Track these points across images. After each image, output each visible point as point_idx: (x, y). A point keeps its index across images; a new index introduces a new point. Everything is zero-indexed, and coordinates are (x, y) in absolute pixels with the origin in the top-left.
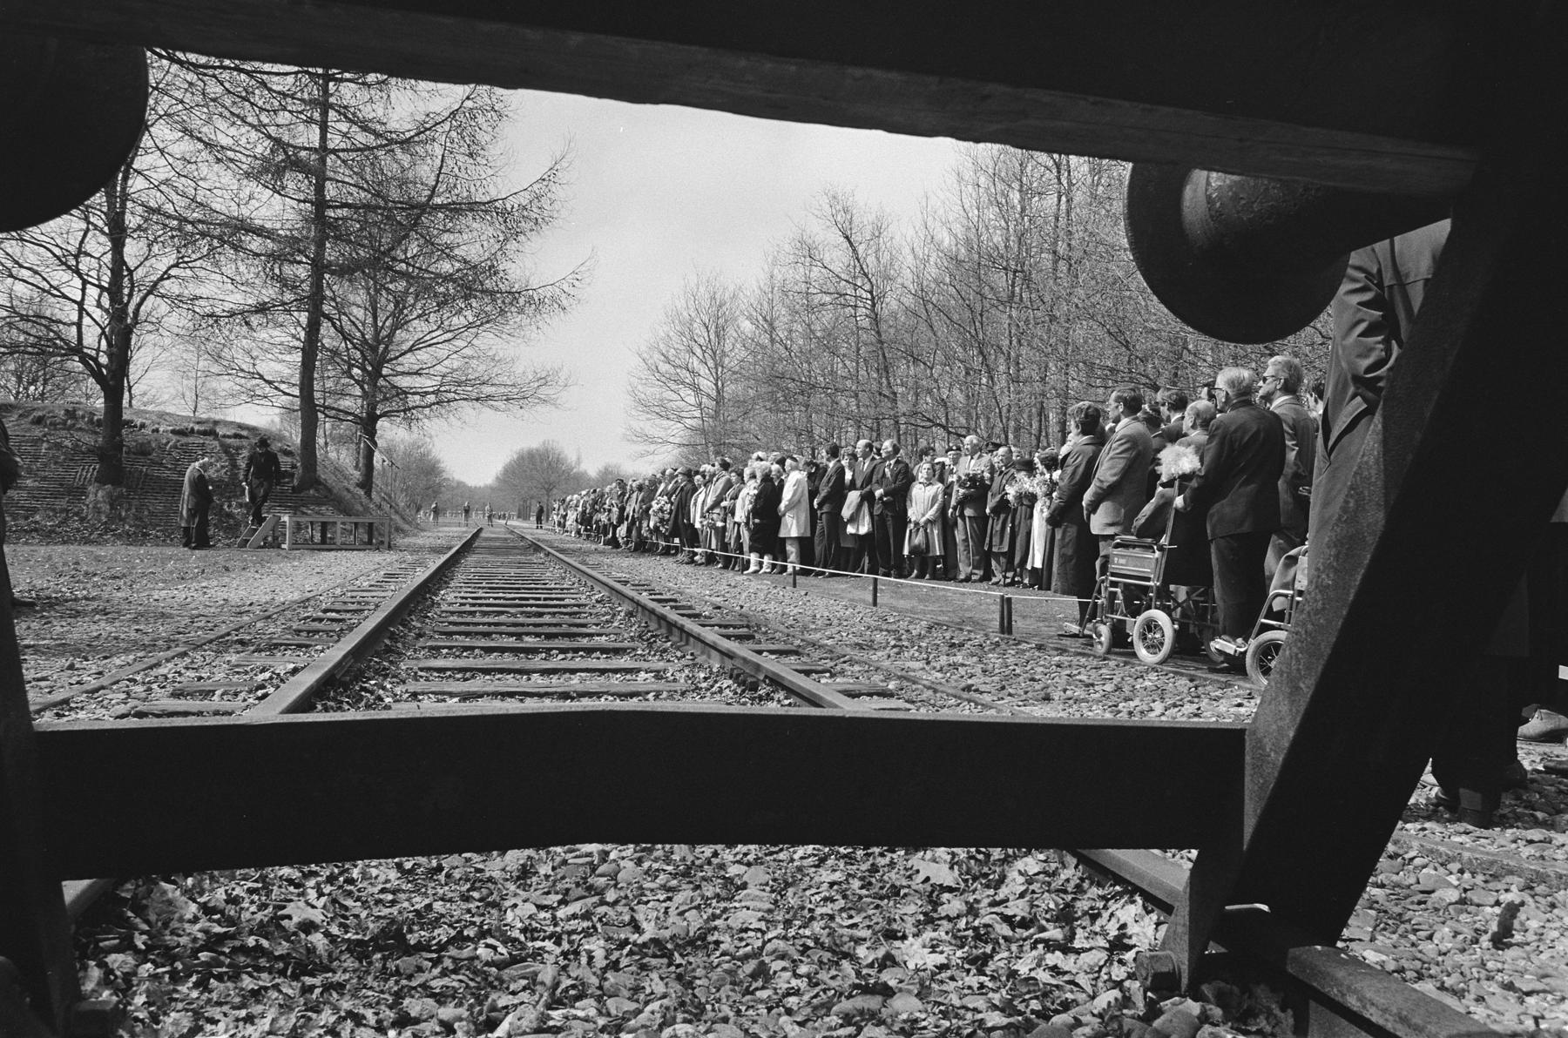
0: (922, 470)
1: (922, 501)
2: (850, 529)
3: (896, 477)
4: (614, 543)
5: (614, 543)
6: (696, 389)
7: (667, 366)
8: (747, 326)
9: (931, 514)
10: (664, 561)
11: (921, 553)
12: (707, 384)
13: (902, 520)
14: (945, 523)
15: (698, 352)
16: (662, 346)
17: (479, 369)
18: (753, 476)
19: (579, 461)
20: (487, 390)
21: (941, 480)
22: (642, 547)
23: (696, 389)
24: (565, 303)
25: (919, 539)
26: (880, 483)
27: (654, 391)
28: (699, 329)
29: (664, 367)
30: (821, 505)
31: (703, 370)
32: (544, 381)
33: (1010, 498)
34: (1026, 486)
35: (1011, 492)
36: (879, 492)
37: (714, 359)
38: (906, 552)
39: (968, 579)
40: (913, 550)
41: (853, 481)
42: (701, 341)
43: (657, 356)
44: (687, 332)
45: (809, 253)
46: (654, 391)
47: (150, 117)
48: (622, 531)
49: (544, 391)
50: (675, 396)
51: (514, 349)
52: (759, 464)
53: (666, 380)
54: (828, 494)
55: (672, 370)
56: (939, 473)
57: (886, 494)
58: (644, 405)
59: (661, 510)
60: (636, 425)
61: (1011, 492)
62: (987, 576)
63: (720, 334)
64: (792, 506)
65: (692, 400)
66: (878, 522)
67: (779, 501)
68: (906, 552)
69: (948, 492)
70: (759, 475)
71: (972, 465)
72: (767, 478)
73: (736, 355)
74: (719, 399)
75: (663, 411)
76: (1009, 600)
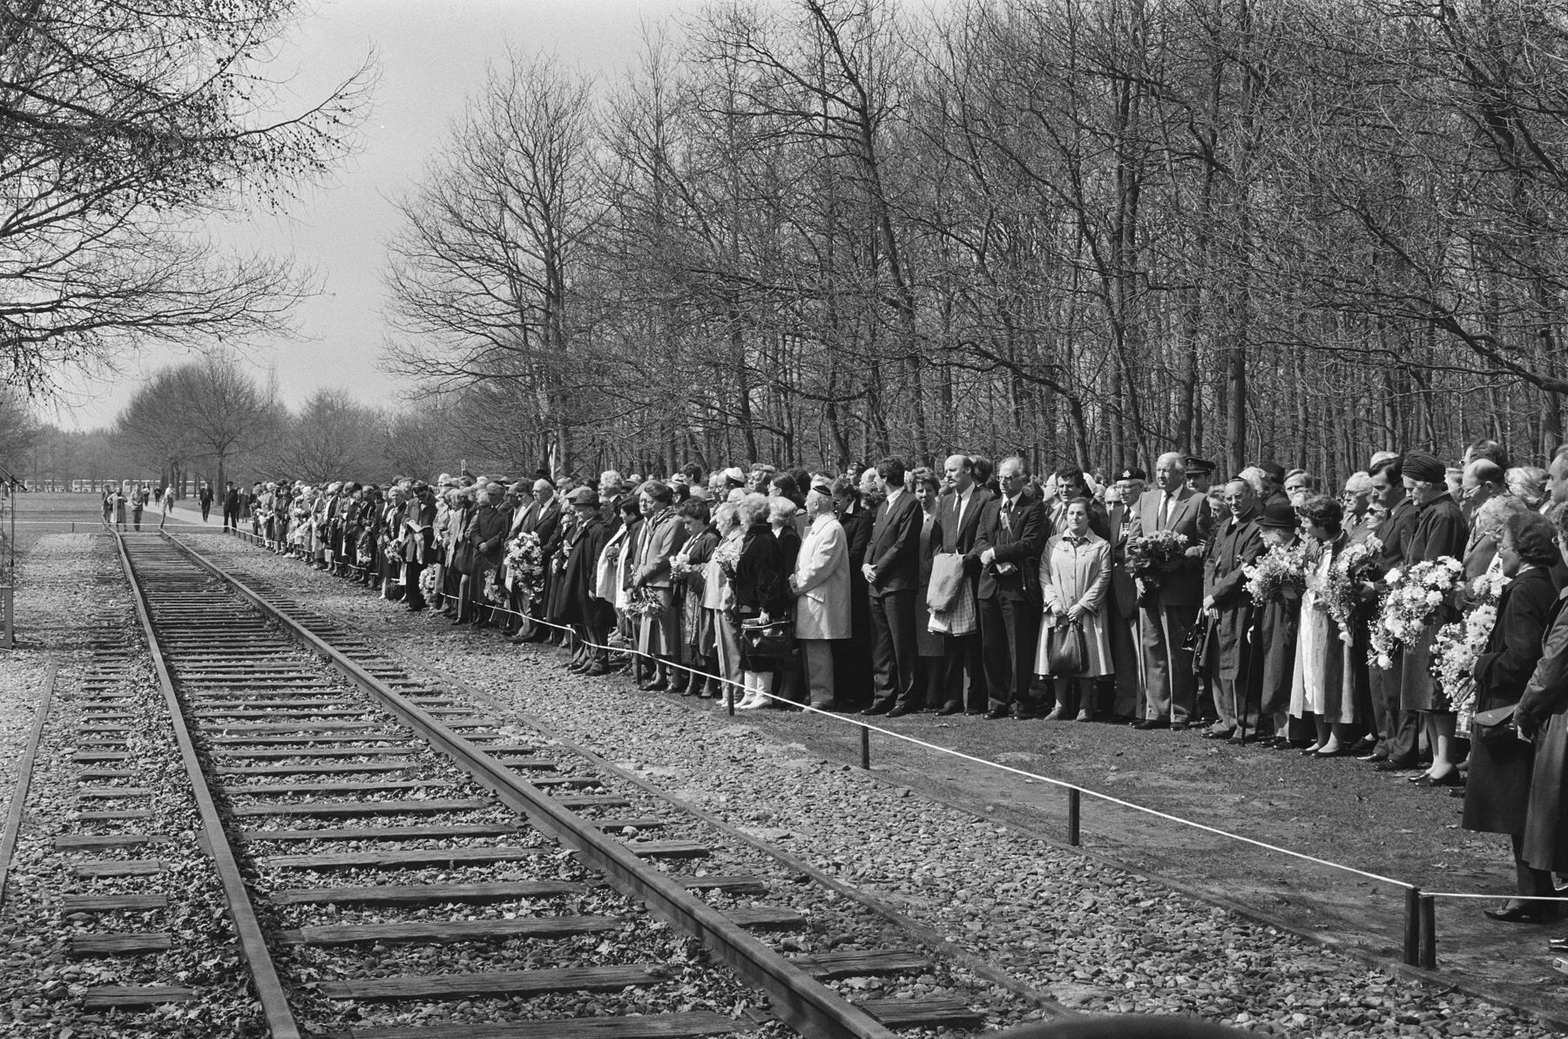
0: (1067, 515)
1: (1069, 572)
2: (935, 624)
3: (1020, 526)
4: (412, 595)
5: (412, 595)
6: (514, 274)
7: (458, 231)
8: (606, 156)
9: (1087, 598)
10: (528, 654)
11: (1069, 672)
12: (531, 262)
13: (1034, 607)
14: (1114, 607)
15: (515, 202)
16: (448, 193)
17: (142, 267)
18: (735, 522)
19: (273, 388)
20: (159, 305)
21: (1105, 533)
22: (478, 619)
23: (514, 274)
24: (322, 154)
25: (1066, 647)
26: (990, 540)
27: (431, 278)
28: (515, 161)
29: (453, 234)
30: (881, 580)
31: (525, 238)
32: (257, 284)
33: (1251, 587)
34: (1285, 563)
35: (1255, 577)
36: (987, 555)
37: (546, 218)
38: (1042, 668)
39: (1162, 722)
40: (1057, 666)
41: (937, 532)
42: (523, 186)
43: (438, 211)
44: (493, 170)
45: (740, 32)
46: (431, 278)
47: (18, 405)
48: (429, 577)
49: (260, 305)
50: (476, 287)
51: (211, 231)
52: (741, 499)
53: (455, 256)
54: (889, 559)
55: (466, 237)
56: (1097, 522)
57: (1000, 558)
58: (420, 305)
59: (527, 556)
60: (405, 342)
61: (1255, 577)
62: (1202, 711)
63: (555, 167)
64: (816, 581)
65: (505, 292)
66: (989, 613)
67: (791, 567)
68: (1042, 668)
69: (1116, 554)
70: (744, 519)
71: (1156, 516)
72: (760, 525)
73: (585, 204)
74: (556, 294)
75: (448, 313)
76: (1429, 901)
